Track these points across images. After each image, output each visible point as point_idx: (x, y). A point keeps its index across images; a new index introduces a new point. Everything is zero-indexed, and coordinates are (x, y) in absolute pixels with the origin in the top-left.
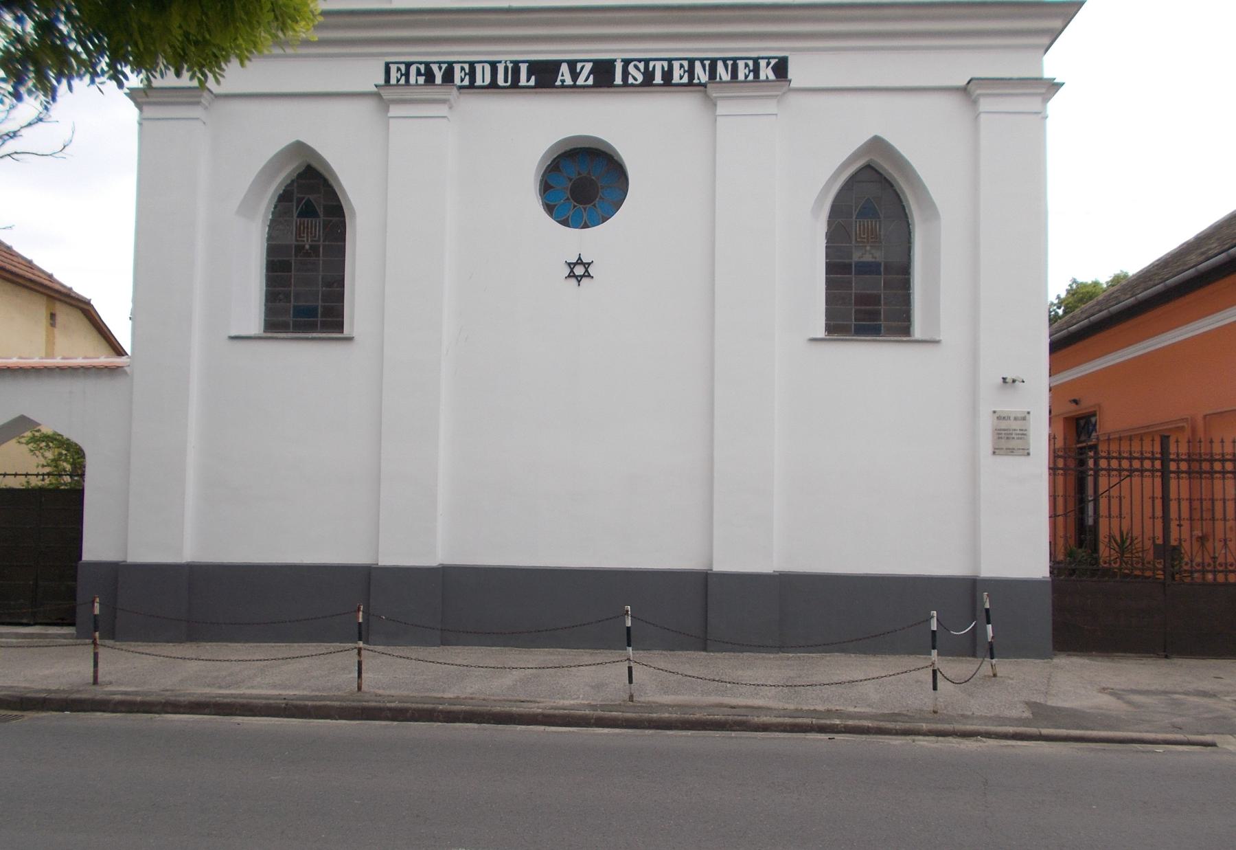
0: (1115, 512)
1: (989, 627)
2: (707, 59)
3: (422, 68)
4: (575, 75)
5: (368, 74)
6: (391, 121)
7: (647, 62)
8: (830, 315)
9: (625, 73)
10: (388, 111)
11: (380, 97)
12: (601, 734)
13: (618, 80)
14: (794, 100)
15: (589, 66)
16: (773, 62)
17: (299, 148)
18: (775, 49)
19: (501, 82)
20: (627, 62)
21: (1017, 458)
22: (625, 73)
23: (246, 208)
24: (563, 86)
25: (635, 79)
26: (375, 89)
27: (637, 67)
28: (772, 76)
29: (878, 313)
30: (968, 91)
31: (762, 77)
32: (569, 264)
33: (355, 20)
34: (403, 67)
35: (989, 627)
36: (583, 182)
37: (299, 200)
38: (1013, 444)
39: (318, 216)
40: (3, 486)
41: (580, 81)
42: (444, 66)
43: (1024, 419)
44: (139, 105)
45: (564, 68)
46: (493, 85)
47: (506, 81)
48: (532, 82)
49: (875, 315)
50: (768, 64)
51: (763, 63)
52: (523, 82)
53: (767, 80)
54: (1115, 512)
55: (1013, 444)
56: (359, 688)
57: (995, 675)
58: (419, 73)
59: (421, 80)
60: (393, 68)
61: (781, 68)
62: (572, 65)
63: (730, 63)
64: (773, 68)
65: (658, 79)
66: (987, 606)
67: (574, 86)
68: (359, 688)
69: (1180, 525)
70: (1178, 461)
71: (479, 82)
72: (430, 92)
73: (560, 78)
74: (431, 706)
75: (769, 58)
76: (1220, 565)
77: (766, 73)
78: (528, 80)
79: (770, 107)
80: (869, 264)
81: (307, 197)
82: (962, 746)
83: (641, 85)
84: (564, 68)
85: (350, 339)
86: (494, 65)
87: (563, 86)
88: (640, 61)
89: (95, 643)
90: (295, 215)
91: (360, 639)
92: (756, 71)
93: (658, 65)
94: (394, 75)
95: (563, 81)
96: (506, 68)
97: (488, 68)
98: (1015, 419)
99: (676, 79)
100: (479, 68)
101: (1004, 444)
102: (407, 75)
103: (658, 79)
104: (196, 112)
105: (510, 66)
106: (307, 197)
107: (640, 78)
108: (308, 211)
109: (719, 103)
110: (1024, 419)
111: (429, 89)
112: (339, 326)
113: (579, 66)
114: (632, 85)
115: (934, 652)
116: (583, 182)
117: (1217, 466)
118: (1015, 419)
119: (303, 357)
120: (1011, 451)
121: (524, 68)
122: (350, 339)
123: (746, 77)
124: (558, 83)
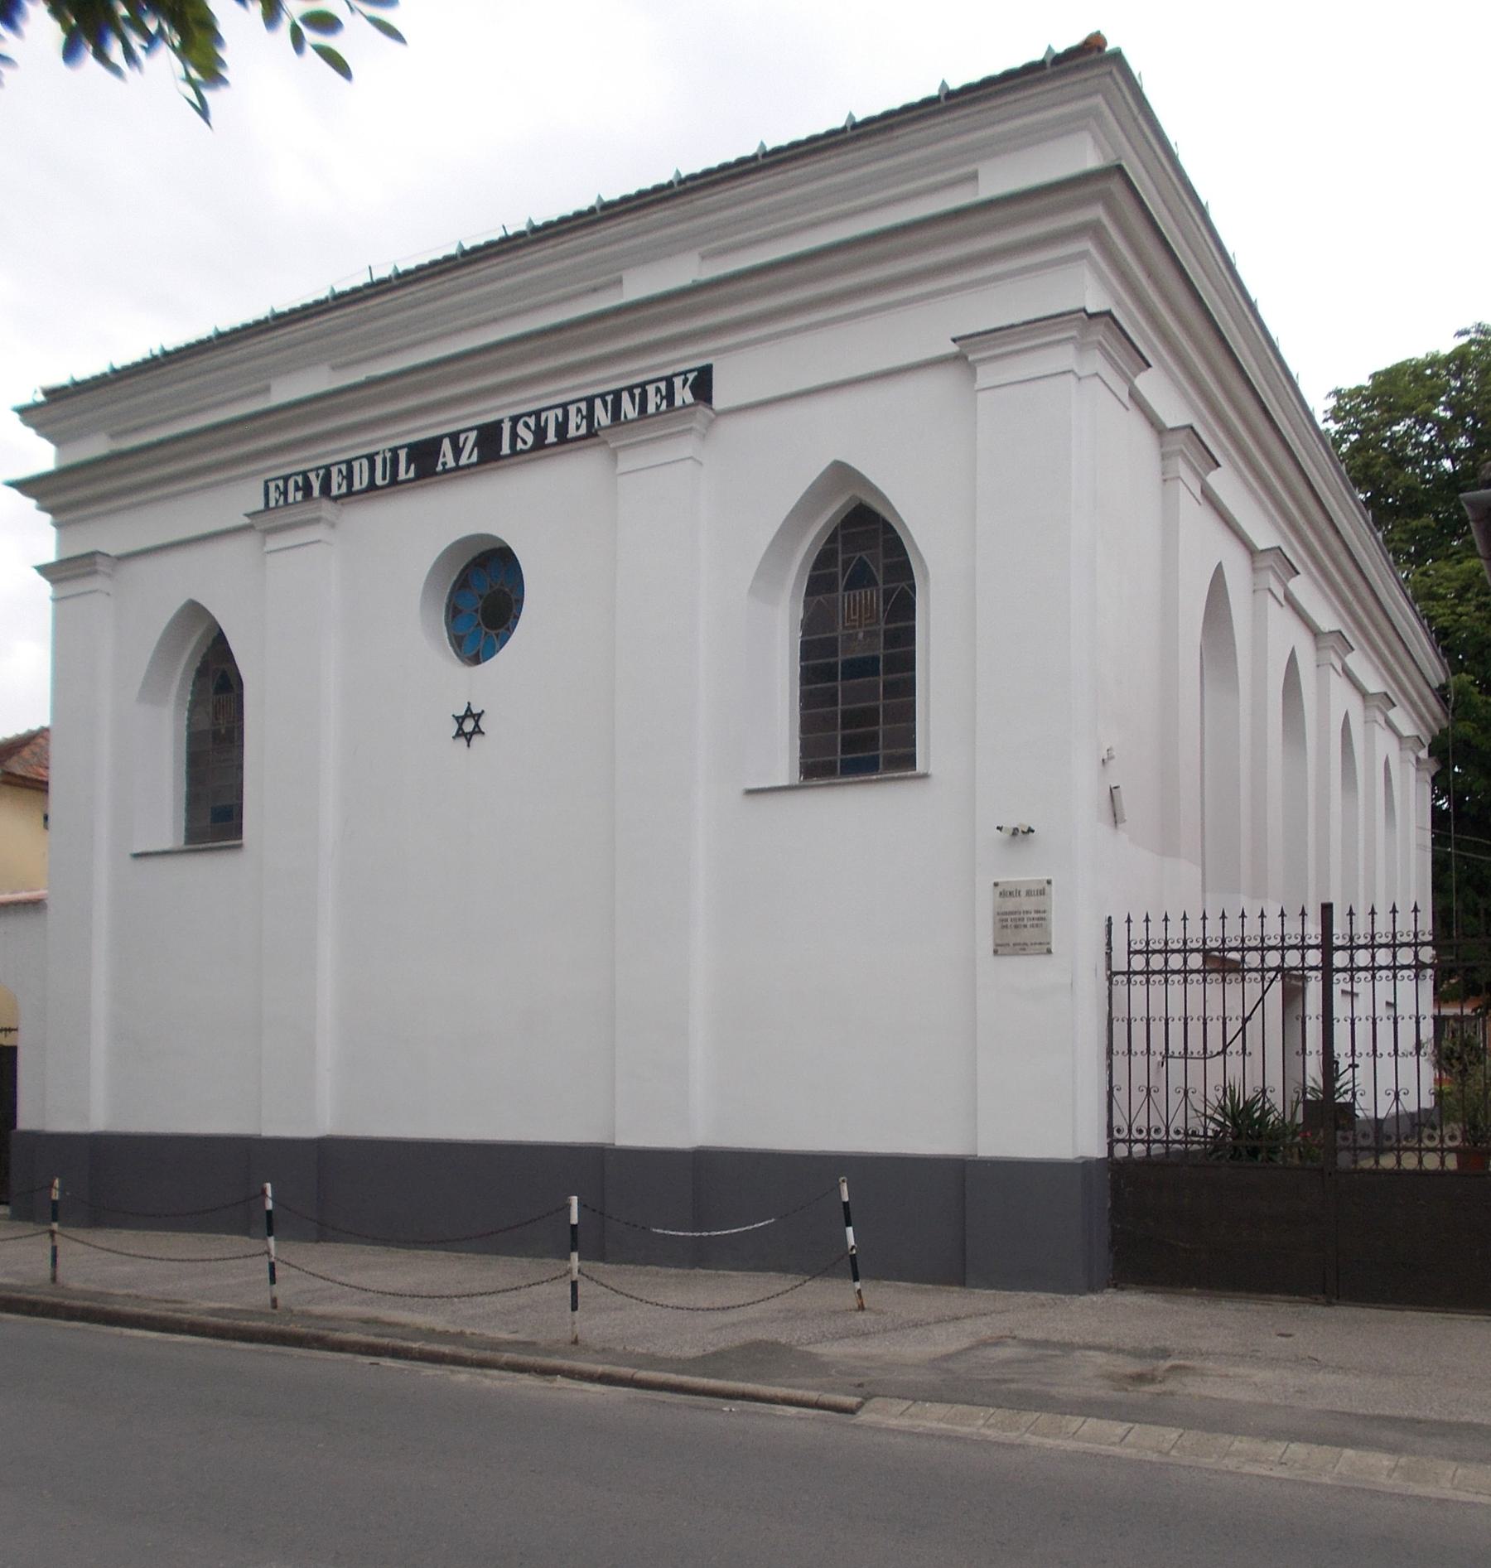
0: (1139, 1044)
1: (850, 1230)
2: (608, 393)
3: (300, 479)
4: (457, 451)
5: (250, 496)
6: (981, 395)
7: (537, 414)
8: (806, 749)
9: (514, 435)
10: (264, 543)
11: (265, 522)
12: (130, 1337)
13: (506, 449)
14: (728, 429)
15: (473, 435)
16: (691, 377)
17: (841, 474)
18: (688, 358)
19: (379, 482)
20: (515, 420)
21: (1031, 958)
22: (514, 435)
23: (150, 691)
24: (446, 471)
25: (525, 442)
26: (247, 521)
27: (527, 425)
28: (689, 399)
29: (874, 737)
30: (968, 353)
31: (678, 402)
32: (457, 718)
33: (152, 455)
34: (281, 483)
35: (850, 1230)
36: (484, 597)
37: (846, 563)
38: (1027, 935)
39: (873, 582)
40: (5, 1043)
41: (463, 461)
42: (321, 472)
43: (1042, 892)
44: (54, 582)
45: (446, 445)
46: (592, 433)
47: (384, 478)
48: (412, 474)
49: (871, 740)
50: (685, 381)
51: (678, 382)
52: (402, 476)
53: (296, 502)
54: (1139, 1044)
55: (1027, 935)
56: (54, 1279)
57: (862, 1308)
58: (297, 488)
59: (299, 496)
60: (272, 486)
61: (703, 385)
62: (454, 437)
63: (637, 391)
64: (691, 387)
65: (551, 437)
66: (846, 1199)
67: (458, 468)
68: (54, 1279)
69: (1354, 1066)
70: (1352, 948)
71: (357, 486)
72: (307, 511)
73: (441, 460)
74: (56, 1300)
75: (685, 373)
76: (1177, 1132)
77: (684, 395)
78: (407, 471)
79: (686, 447)
80: (864, 660)
81: (858, 555)
82: (487, 1382)
83: (534, 449)
84: (446, 445)
85: (925, 776)
86: (371, 458)
87: (446, 471)
88: (529, 414)
89: (52, 1233)
90: (841, 589)
91: (55, 1220)
92: (670, 396)
93: (551, 415)
94: (273, 495)
95: (444, 464)
96: (384, 460)
97: (365, 462)
98: (1029, 893)
99: (572, 432)
100: (356, 465)
101: (1011, 936)
102: (285, 493)
103: (551, 437)
104: (97, 583)
105: (388, 455)
106: (858, 555)
107: (530, 439)
108: (860, 578)
109: (980, 370)
110: (1042, 892)
111: (308, 506)
112: (909, 761)
113: (462, 438)
114: (522, 452)
115: (575, 1256)
116: (484, 597)
117: (1405, 956)
118: (1029, 893)
119: (857, 809)
120: (1021, 949)
121: (403, 454)
122: (925, 776)
123: (658, 407)
124: (440, 468)
